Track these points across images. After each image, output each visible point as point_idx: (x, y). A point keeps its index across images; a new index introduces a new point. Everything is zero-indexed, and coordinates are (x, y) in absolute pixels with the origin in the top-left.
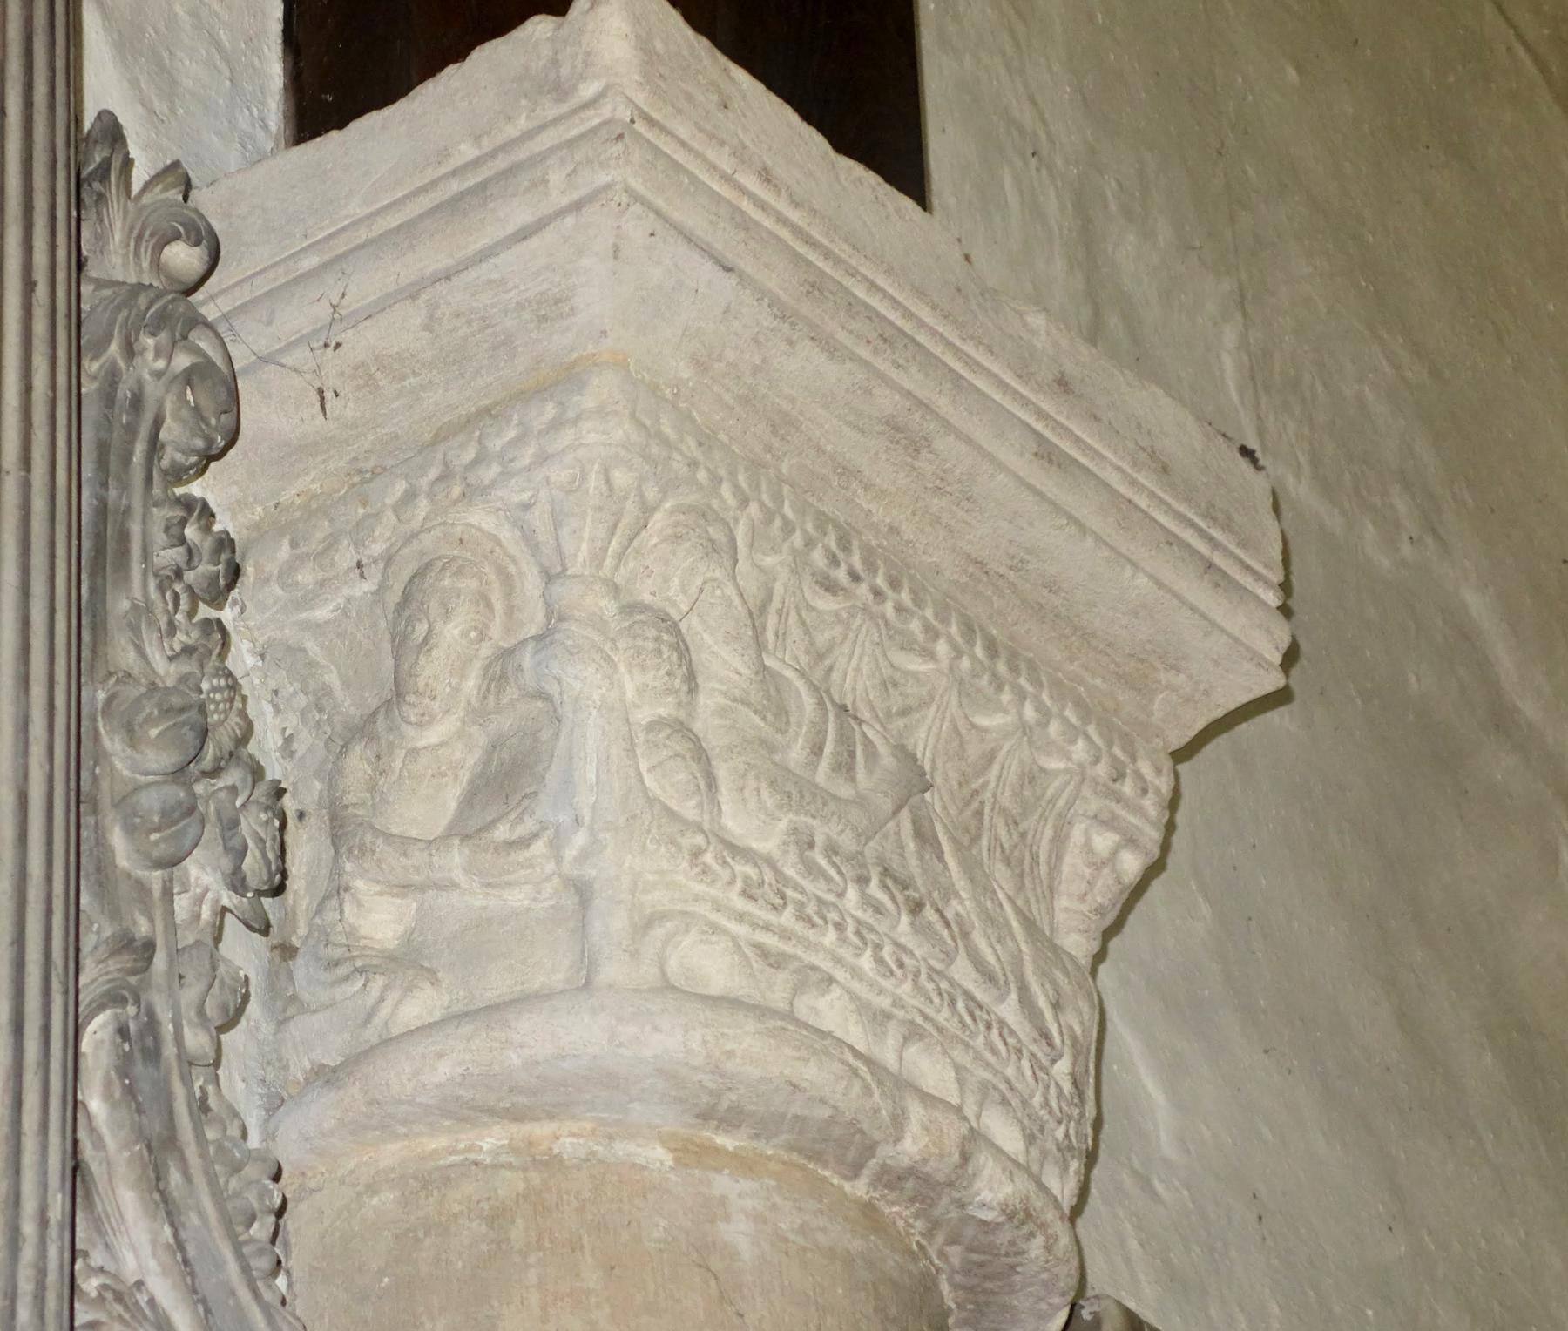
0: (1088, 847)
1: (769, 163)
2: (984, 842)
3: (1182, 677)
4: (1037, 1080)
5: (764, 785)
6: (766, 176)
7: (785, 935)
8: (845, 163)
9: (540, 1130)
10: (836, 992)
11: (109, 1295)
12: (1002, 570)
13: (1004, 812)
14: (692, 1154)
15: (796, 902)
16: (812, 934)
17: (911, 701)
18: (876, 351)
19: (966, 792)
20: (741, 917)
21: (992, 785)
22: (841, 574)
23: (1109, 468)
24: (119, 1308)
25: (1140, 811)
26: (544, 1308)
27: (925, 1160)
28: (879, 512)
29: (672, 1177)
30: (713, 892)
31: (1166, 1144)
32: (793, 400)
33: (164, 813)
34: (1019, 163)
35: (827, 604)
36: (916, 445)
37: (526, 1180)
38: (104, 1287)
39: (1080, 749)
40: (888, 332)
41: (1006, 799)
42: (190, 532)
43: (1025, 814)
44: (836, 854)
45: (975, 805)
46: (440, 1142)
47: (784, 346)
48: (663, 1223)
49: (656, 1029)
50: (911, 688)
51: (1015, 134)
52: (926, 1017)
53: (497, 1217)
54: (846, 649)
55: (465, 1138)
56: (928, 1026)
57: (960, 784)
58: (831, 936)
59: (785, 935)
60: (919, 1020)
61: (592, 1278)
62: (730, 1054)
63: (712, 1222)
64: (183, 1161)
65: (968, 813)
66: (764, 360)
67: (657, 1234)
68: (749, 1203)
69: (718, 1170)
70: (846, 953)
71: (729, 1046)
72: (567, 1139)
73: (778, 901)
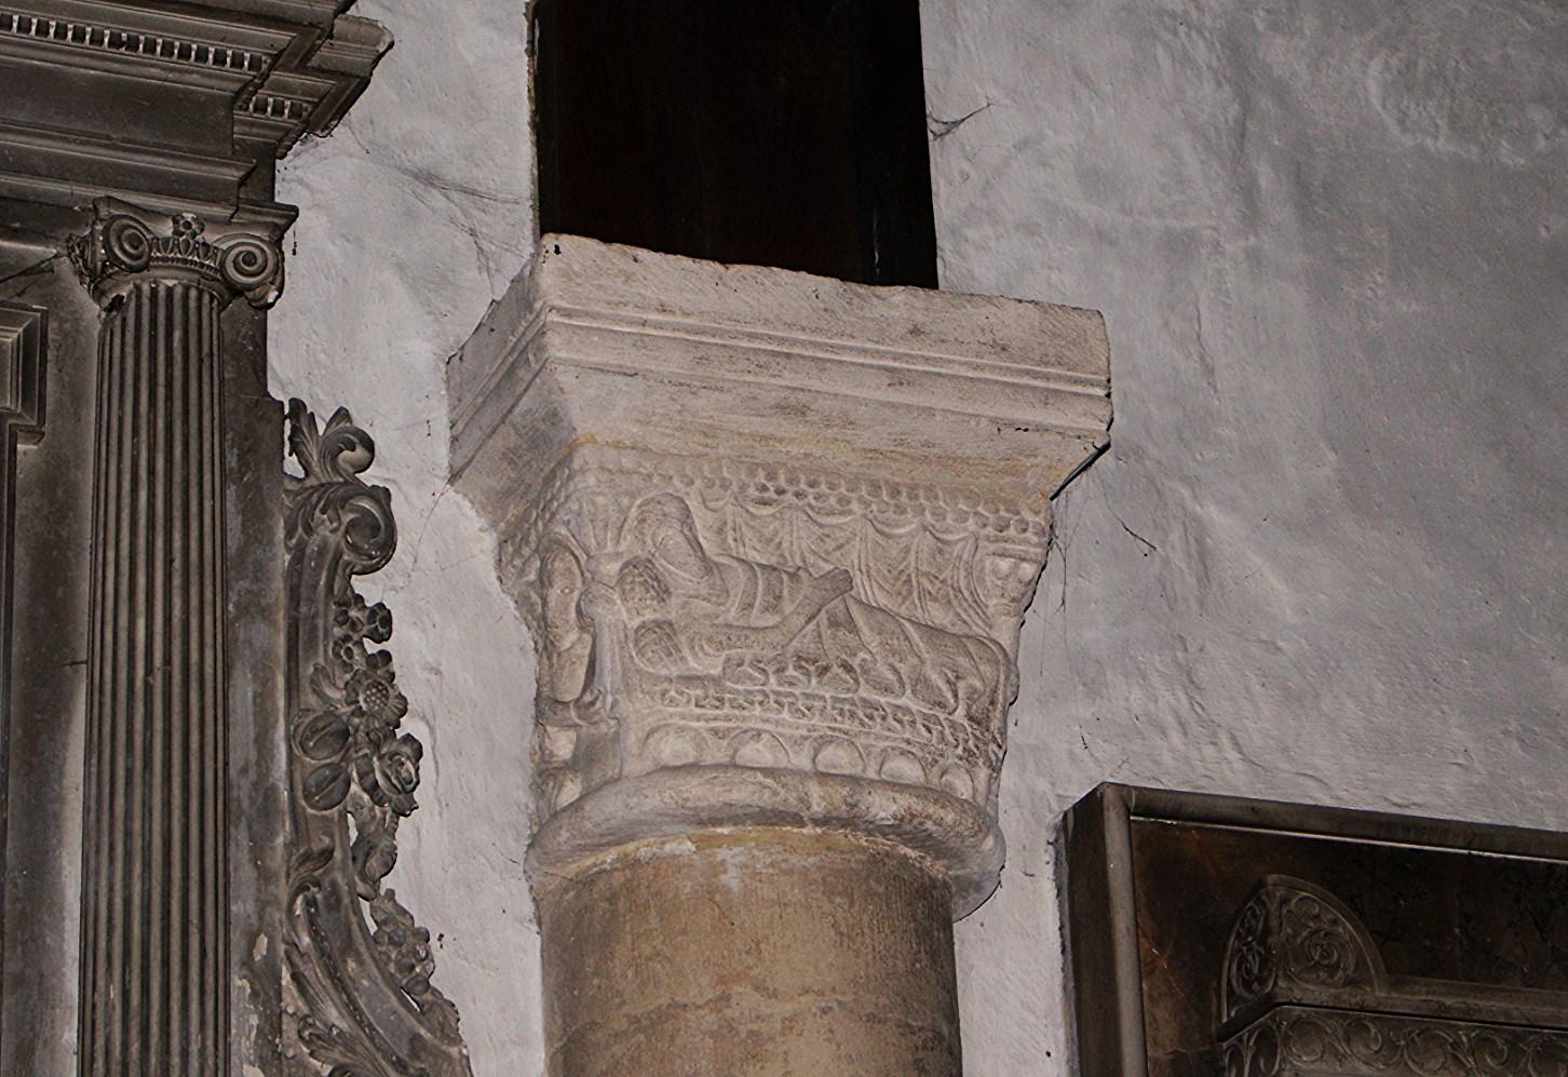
0: (995, 572)
1: (664, 299)
2: (915, 594)
3: (1040, 458)
4: (930, 732)
5: (703, 642)
6: (663, 309)
7: (728, 719)
8: (735, 268)
9: (631, 847)
10: (765, 736)
11: (314, 1038)
12: (892, 448)
13: (926, 574)
14: (702, 843)
15: (730, 700)
16: (746, 713)
17: (841, 541)
18: (757, 374)
19: (895, 573)
20: (698, 719)
21: (913, 564)
22: (771, 494)
23: (957, 367)
24: (321, 1043)
25: (1027, 542)
26: (633, 944)
27: (829, 812)
28: (794, 450)
29: (695, 857)
30: (679, 709)
31: (1290, 617)
32: (711, 417)
33: (317, 786)
34: (1168, 37)
35: (766, 511)
36: (802, 411)
37: (625, 876)
38: (311, 1034)
39: (971, 524)
40: (763, 359)
41: (924, 568)
42: (353, 613)
43: (940, 571)
44: (760, 662)
45: (904, 578)
46: (589, 862)
47: (691, 396)
48: (690, 884)
49: (646, 797)
50: (838, 534)
51: (1167, 20)
52: (834, 729)
53: (613, 899)
54: (787, 529)
55: (601, 857)
56: (837, 734)
57: (889, 571)
58: (758, 710)
59: (728, 719)
60: (830, 733)
61: (654, 923)
62: (687, 800)
63: (716, 876)
64: (358, 954)
65: (899, 583)
66: (682, 405)
67: (687, 890)
68: (737, 860)
69: (720, 847)
70: (773, 716)
71: (685, 796)
72: (642, 849)
73: (717, 704)
